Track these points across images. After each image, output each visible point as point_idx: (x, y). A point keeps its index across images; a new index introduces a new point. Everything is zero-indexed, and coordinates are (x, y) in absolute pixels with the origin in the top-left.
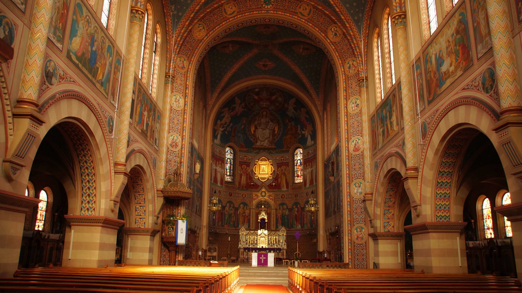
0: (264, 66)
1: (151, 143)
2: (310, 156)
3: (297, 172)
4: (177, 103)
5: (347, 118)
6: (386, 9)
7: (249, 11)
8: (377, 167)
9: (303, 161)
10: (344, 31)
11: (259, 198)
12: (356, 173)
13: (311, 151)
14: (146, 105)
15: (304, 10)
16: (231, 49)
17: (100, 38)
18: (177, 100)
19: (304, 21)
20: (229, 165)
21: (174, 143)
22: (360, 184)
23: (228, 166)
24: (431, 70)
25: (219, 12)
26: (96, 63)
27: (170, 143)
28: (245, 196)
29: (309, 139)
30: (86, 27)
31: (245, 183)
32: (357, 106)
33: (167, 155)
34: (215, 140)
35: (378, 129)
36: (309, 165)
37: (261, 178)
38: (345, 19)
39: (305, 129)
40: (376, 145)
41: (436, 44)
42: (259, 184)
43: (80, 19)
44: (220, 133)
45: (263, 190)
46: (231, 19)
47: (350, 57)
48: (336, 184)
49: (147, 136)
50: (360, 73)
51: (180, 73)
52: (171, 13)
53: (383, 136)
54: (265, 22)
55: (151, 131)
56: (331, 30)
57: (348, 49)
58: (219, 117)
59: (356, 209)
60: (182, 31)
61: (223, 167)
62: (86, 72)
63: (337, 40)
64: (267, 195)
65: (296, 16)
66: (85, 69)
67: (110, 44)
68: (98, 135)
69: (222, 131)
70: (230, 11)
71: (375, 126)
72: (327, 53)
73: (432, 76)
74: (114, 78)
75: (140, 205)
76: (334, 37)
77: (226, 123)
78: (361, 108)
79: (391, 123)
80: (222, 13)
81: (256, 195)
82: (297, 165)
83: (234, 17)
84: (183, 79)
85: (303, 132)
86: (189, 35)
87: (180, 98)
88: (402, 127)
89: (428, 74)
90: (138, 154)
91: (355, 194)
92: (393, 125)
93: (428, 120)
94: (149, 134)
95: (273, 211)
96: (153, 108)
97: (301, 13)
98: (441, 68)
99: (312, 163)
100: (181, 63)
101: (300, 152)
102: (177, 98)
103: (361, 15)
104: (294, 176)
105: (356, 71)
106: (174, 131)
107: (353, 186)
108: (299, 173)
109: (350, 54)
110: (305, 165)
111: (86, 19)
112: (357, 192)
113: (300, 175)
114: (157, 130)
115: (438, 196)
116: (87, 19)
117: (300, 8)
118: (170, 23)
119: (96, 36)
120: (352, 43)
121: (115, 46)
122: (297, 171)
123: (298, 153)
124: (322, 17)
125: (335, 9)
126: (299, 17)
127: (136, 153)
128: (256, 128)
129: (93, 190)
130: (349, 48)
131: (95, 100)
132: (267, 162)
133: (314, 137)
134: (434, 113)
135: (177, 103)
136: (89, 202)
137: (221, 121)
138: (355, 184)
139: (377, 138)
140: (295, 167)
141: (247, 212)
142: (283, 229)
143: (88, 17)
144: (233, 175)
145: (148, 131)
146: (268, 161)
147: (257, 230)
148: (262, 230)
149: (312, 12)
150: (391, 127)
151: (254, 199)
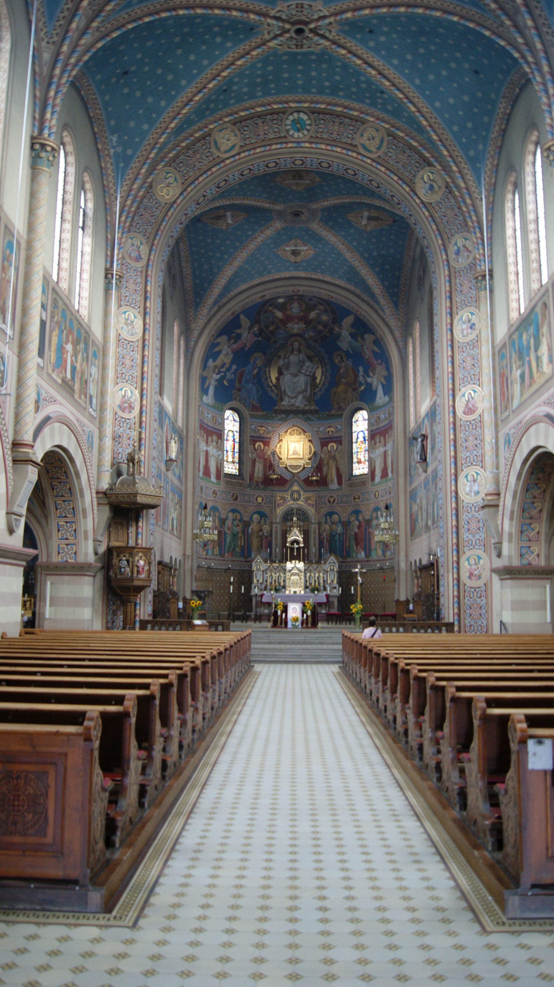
0: (295, 253)
10: (448, 180)
12: (468, 454)
16: (230, 221)
18: (129, 321)
21: (126, 403)
25: (204, 147)
27: (118, 403)
28: (263, 500)
29: (380, 392)
32: (471, 328)
33: (114, 426)
36: (380, 442)
40: (508, 402)
42: (287, 476)
44: (213, 383)
45: (296, 488)
46: (228, 162)
49: (73, 390)
50: (478, 262)
52: (112, 151)
53: (521, 384)
56: (423, 178)
60: (135, 186)
63: (434, 198)
71: (507, 366)
76: (427, 192)
77: (223, 365)
78: (480, 332)
79: (538, 359)
83: (233, 156)
84: (139, 280)
85: (369, 380)
87: (135, 317)
90: (57, 425)
91: (467, 494)
92: (542, 362)
94: (77, 387)
95: (314, 527)
96: (83, 338)
97: (364, 147)
104: (352, 462)
105: (471, 260)
106: (125, 381)
109: (459, 226)
110: (373, 441)
112: (471, 491)
117: (362, 135)
118: (109, 172)
120: (462, 204)
127: (54, 422)
128: (280, 373)
130: (458, 214)
133: (388, 389)
138: (466, 477)
141: (266, 528)
145: (76, 380)
148: (293, 562)
149: (385, 144)
151: (279, 505)
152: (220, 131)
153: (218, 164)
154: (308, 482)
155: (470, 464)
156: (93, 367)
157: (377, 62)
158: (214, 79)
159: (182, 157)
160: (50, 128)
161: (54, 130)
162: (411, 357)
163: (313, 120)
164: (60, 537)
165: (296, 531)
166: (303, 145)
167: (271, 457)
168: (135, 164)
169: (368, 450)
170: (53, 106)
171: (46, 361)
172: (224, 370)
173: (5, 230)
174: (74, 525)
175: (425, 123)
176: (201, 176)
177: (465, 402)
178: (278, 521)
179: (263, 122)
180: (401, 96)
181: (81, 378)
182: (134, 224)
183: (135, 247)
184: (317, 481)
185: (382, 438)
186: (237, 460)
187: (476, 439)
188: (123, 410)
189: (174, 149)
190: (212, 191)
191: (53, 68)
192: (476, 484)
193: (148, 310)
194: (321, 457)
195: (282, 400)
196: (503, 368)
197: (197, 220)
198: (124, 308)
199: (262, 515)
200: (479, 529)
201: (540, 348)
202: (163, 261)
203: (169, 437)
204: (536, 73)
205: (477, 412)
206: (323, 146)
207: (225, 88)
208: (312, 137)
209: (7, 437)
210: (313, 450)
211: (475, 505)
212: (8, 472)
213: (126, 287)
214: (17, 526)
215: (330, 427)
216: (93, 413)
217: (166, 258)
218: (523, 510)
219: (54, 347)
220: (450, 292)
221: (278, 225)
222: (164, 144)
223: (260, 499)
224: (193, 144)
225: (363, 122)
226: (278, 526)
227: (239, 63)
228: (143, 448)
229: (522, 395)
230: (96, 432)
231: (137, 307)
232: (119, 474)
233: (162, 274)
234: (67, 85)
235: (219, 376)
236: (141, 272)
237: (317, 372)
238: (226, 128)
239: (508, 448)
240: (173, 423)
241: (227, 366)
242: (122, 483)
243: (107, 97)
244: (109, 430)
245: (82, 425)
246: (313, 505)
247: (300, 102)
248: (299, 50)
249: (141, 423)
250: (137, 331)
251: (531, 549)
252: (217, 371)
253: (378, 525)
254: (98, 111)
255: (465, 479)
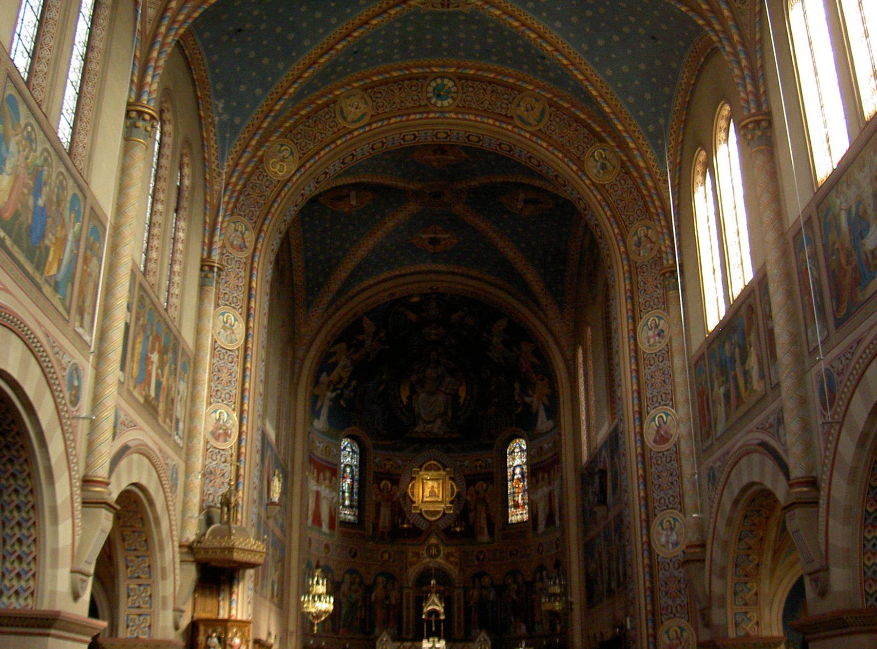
0: (433, 242)
1: (167, 429)
2: (544, 457)
3: (514, 497)
4: (229, 332)
5: (637, 365)
6: (721, 107)
7: (401, 113)
8: (714, 481)
9: (527, 469)
10: (624, 158)
11: (424, 561)
12: (662, 495)
13: (548, 443)
14: (157, 338)
15: (527, 111)
16: (354, 202)
17: (54, 177)
18: (228, 325)
19: (528, 135)
20: (349, 481)
21: (221, 428)
22: (672, 522)
23: (346, 484)
24: (840, 248)
25: (327, 117)
26: (43, 236)
27: (211, 429)
28: (390, 557)
29: (542, 415)
30: (24, 150)
31: (387, 524)
32: (659, 335)
33: (204, 458)
34: (316, 423)
35: (712, 391)
36: (543, 479)
37: (426, 512)
38: (627, 131)
39: (530, 392)
40: (710, 427)
41: (848, 186)
42: (423, 526)
43: (11, 132)
44: (327, 403)
45: (433, 540)
46: (356, 133)
47: (639, 219)
48: (612, 523)
49: (157, 412)
50: (664, 256)
51: (236, 259)
52: (217, 119)
53: (725, 406)
54: (437, 138)
55: (167, 399)
56: (593, 155)
57: (635, 199)
58: (325, 365)
59: (666, 584)
60: (243, 161)
61: (335, 487)
62: (21, 258)
63: (608, 179)
64: (442, 552)
65: (510, 124)
66: (19, 251)
67: (77, 192)
68: (46, 412)
69: (331, 400)
70: (355, 114)
71: (706, 382)
72: (585, 210)
73: (843, 262)
74: (84, 271)
75: (140, 582)
76: (599, 172)
77: (341, 380)
78: (670, 339)
79: (746, 374)
80: (335, 120)
81: (417, 555)
82: (513, 479)
83: (363, 127)
84: (243, 274)
85: (527, 399)
86: (258, 170)
87: (236, 320)
88: (774, 381)
89: (833, 254)
90: (135, 456)
91: (663, 546)
92: (751, 377)
93: (836, 364)
94: (161, 408)
95: (457, 593)
96: (171, 345)
97: (521, 118)
98: (863, 241)
99: (549, 475)
100: (238, 237)
101: (521, 447)
102: (229, 321)
103: (662, 121)
104: (507, 507)
105: (654, 253)
106: (220, 400)
107: (655, 527)
108: (520, 498)
109: (639, 212)
110: (534, 479)
111: (25, 133)
112: (667, 542)
113: (520, 501)
114: (179, 397)
115: (869, 546)
116: (28, 132)
117: (519, 105)
118: (212, 143)
119: (45, 173)
120: (642, 187)
121: (88, 195)
122: (514, 493)
123: (517, 450)
124: (570, 126)
125: (602, 108)
126: (516, 126)
127: (132, 453)
128: (413, 392)
129: (29, 546)
130: (637, 198)
131: (40, 325)
132: (442, 472)
133: (553, 411)
134: (851, 348)
135: (229, 332)
136: (19, 575)
137: (329, 375)
138: (661, 524)
139: (711, 409)
140: (510, 484)
141: (394, 594)
142: (483, 635)
143: (29, 128)
144: (360, 505)
145: (161, 399)
146: (444, 470)
147: (421, 641)
148: (431, 639)
149: (547, 116)
150: (746, 382)
151: (412, 564)
152: (348, 98)
153: (345, 135)
154: (448, 534)
155: (665, 507)
156: (182, 382)
157: (536, 23)
158: (343, 39)
159: (300, 127)
160: (150, 93)
161: (154, 95)
162: (581, 371)
163: (459, 87)
164: (130, 604)
165: (435, 598)
166: (447, 115)
167: (401, 499)
168: (243, 135)
169: (527, 490)
170: (155, 68)
171: (127, 375)
172: (340, 386)
173: (91, 214)
174: (149, 588)
175: (594, 93)
176: (322, 149)
177: (656, 429)
178: (410, 585)
179: (400, 89)
180: (565, 62)
181: (167, 396)
182: (238, 206)
183: (238, 233)
184: (461, 532)
185: (546, 475)
186: (355, 503)
187: (671, 474)
188: (217, 437)
189: (291, 118)
190: (335, 167)
191: (158, 26)
192: (674, 533)
193: (252, 312)
194: (466, 500)
195: (415, 425)
196: (701, 384)
197: (313, 200)
198: (222, 309)
199: (390, 577)
200: (680, 592)
201: (748, 361)
202: (273, 250)
203: (271, 473)
204: (725, 43)
205: (671, 440)
206: (472, 117)
207: (355, 49)
208: (458, 106)
209: (78, 471)
210: (456, 490)
211: (674, 560)
212: (76, 517)
213: (226, 282)
214: (84, 589)
215: (478, 460)
216: (179, 441)
217: (276, 247)
218: (736, 566)
219: (137, 357)
220: (632, 291)
221: (413, 207)
222: (280, 112)
223: (386, 556)
224: (316, 111)
225: (521, 90)
226: (411, 591)
227: (374, 22)
228: (241, 487)
229: (727, 419)
230: (182, 466)
231: (238, 307)
232: (209, 521)
233: (271, 266)
234: (173, 45)
235: (334, 394)
236: (245, 263)
237: (461, 389)
238: (355, 95)
239: (713, 485)
240: (276, 455)
241: (345, 381)
242: (214, 534)
243: (215, 58)
244: (198, 463)
245: (166, 457)
246: (456, 564)
247: (444, 66)
248: (445, 10)
249: (239, 455)
250: (238, 337)
251: (749, 615)
252: (332, 387)
253: (544, 590)
254: (203, 73)
255: (660, 528)
